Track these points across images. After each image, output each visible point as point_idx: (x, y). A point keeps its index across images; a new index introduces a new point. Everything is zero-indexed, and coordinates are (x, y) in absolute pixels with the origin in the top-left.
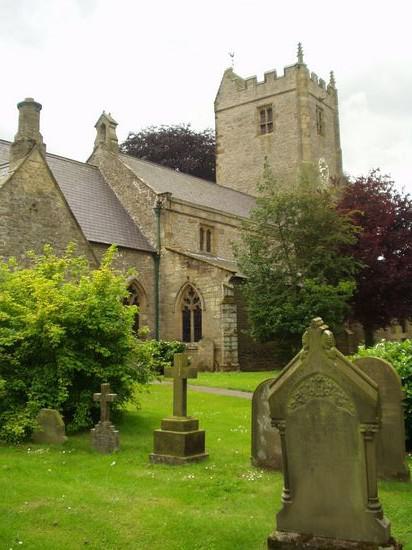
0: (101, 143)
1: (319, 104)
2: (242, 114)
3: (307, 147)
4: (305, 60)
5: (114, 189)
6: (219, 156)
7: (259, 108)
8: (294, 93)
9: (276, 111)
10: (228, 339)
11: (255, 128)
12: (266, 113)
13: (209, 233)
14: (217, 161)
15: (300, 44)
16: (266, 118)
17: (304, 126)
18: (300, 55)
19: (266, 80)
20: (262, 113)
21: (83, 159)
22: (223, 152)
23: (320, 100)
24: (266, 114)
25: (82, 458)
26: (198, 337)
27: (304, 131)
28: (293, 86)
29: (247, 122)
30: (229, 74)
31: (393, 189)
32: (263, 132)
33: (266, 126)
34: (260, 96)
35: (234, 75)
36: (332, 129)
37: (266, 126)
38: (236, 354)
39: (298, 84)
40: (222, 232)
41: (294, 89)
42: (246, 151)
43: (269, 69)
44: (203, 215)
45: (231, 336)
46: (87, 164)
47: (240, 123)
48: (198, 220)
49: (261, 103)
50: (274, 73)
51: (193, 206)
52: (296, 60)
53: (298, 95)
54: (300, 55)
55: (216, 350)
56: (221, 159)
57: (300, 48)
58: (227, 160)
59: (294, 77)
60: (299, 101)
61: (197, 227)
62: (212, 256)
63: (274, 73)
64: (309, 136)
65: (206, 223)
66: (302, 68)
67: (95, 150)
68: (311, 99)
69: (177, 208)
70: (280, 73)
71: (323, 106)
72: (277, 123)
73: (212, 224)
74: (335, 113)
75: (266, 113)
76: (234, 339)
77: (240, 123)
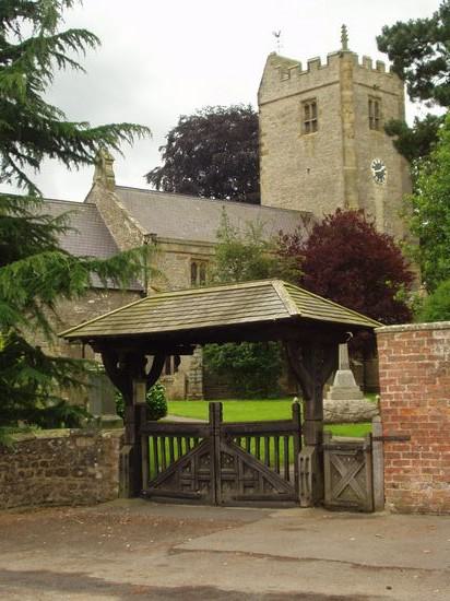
0: (99, 180)
1: (374, 93)
2: (286, 109)
3: (351, 150)
4: (351, 46)
5: (109, 227)
6: (263, 158)
7: (303, 102)
8: (338, 85)
9: (320, 107)
10: (193, 372)
11: (299, 126)
12: (310, 106)
14: (262, 164)
15: (344, 27)
16: (311, 114)
17: (347, 126)
18: (344, 39)
19: (309, 70)
20: (307, 108)
21: (81, 199)
23: (375, 88)
24: (311, 108)
25: (148, 503)
26: (176, 370)
27: (347, 132)
28: (337, 78)
29: (291, 119)
30: (273, 60)
32: (308, 131)
33: (311, 125)
34: (313, 86)
35: (280, 59)
37: (311, 125)
38: (200, 385)
39: (341, 76)
41: (337, 82)
42: (290, 152)
43: (312, 56)
44: (195, 250)
45: (195, 370)
46: (85, 203)
47: (283, 119)
48: (189, 256)
49: (305, 97)
50: (318, 61)
51: (181, 243)
52: (339, 47)
53: (342, 89)
54: (344, 39)
55: (187, 382)
56: (265, 163)
57: (344, 32)
58: (271, 163)
59: (337, 67)
60: (342, 97)
61: (187, 263)
63: (318, 61)
64: (353, 137)
65: (199, 257)
66: (346, 57)
67: (94, 185)
68: (360, 90)
69: (164, 247)
70: (324, 62)
71: (381, 94)
72: (321, 121)
75: (310, 106)
76: (199, 372)
77: (283, 119)
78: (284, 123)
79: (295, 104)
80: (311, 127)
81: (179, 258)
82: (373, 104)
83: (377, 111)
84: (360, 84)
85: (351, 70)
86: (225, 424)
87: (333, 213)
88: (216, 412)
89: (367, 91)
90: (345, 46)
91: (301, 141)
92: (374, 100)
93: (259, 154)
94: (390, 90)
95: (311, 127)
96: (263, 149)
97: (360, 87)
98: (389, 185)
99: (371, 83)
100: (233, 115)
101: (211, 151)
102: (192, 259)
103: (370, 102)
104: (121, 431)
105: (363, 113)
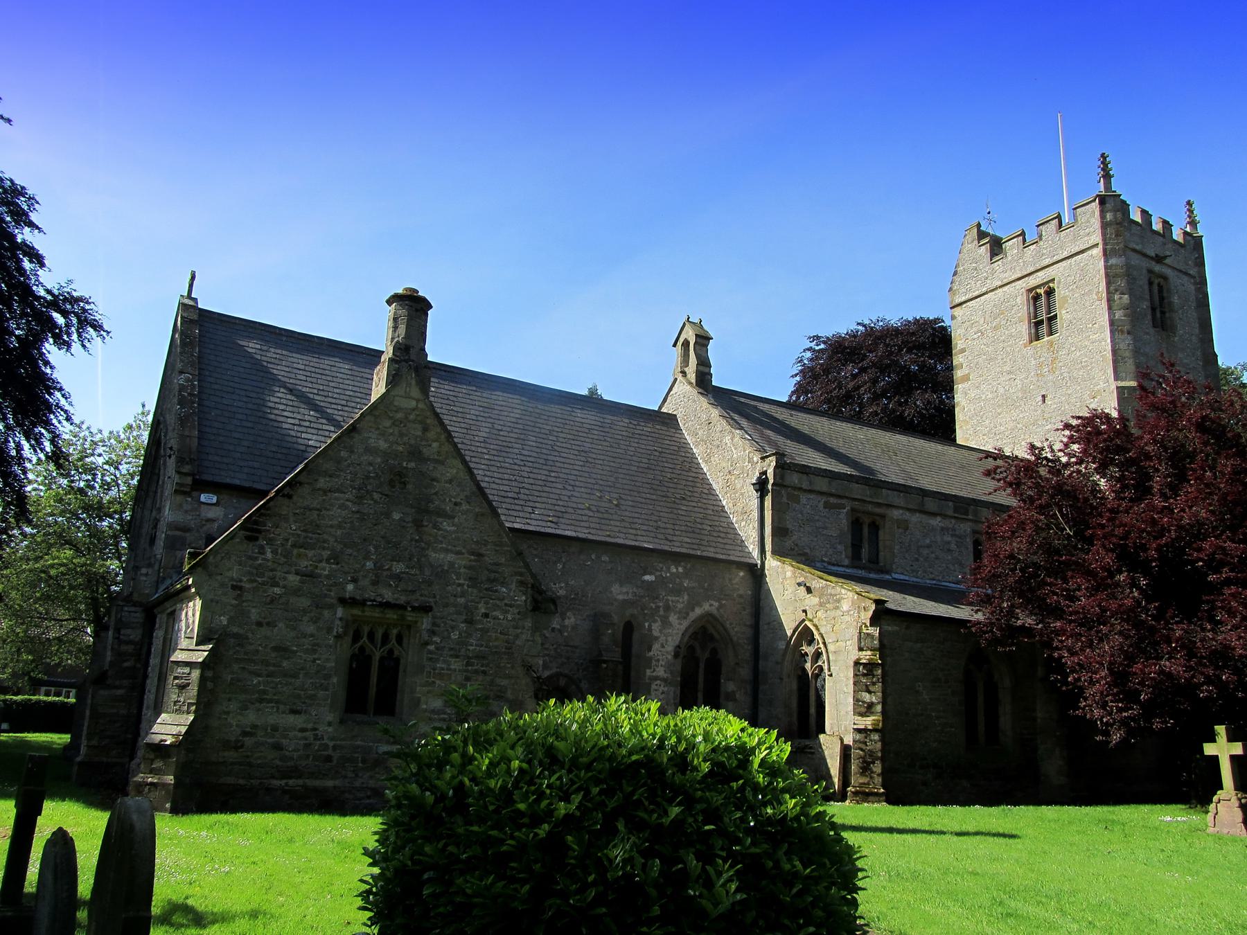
1: (1157, 268)
4: (1116, 187)
7: (1030, 290)
11: (1024, 329)
13: (875, 528)
16: (1044, 310)
18: (1107, 176)
22: (966, 378)
23: (1159, 259)
31: (94, 430)
36: (1193, 315)
40: (904, 525)
42: (1009, 373)
49: (1033, 281)
61: (842, 521)
62: (882, 572)
71: (1168, 272)
73: (878, 510)
74: (1201, 283)
78: (996, 328)
79: (1017, 297)
81: (827, 505)
82: (1156, 288)
83: (1162, 299)
86: (101, 805)
87: (859, 864)
88: (1047, 626)
89: (1146, 264)
90: (1108, 186)
92: (1156, 281)
94: (1181, 267)
95: (1045, 327)
96: (958, 374)
102: (853, 510)
103: (1151, 283)
104: (178, 656)
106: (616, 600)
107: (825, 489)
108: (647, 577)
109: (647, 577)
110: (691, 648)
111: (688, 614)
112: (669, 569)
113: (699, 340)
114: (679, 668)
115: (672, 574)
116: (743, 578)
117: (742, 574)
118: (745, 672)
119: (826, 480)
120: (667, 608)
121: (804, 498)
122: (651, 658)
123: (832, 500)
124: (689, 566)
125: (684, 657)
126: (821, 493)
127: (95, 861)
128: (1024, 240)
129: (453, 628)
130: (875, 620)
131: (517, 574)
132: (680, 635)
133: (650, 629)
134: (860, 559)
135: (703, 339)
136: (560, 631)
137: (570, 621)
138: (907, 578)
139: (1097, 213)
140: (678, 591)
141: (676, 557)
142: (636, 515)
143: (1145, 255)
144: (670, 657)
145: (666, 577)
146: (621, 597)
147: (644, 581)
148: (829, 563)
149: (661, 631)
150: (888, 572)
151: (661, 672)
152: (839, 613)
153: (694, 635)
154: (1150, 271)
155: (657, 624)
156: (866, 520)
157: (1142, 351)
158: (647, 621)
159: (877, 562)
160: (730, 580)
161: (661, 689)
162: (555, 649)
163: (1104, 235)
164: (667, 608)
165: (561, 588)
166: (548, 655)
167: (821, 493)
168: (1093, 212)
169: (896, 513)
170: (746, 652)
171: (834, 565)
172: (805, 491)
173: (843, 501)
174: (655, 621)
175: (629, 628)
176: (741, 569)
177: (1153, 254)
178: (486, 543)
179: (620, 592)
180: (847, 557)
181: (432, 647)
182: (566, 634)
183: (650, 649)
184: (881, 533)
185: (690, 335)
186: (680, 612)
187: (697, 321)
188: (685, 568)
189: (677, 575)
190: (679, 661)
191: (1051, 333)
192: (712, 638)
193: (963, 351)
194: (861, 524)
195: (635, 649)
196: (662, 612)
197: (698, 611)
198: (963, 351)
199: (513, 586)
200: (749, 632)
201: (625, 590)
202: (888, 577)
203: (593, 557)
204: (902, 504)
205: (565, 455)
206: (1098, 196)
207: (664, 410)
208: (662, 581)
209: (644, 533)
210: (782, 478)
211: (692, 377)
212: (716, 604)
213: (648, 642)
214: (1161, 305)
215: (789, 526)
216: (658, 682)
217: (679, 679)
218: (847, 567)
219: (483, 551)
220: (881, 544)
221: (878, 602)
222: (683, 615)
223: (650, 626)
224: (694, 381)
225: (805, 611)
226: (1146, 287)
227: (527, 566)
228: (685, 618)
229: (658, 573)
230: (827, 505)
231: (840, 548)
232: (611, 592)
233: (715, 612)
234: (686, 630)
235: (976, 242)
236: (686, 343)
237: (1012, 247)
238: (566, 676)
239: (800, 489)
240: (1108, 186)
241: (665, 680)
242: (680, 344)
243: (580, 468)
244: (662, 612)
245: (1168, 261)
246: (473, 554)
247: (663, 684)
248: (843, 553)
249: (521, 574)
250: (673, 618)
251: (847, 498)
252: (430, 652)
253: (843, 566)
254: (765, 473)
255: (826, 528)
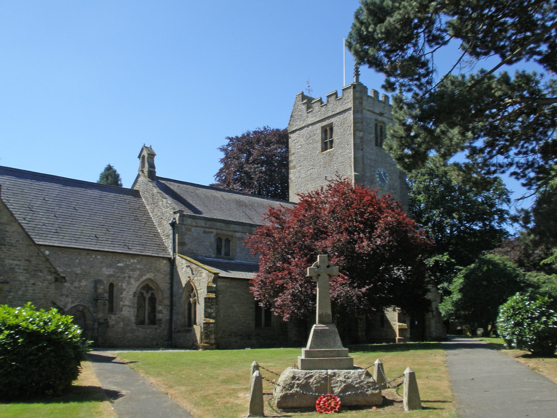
1: (380, 118)
4: (361, 80)
6: (291, 171)
11: (319, 145)
12: (327, 131)
13: (228, 241)
22: (294, 167)
33: (327, 144)
37: (327, 144)
48: (215, 231)
49: (324, 123)
62: (231, 260)
64: (362, 150)
66: (358, 89)
80: (329, 146)
81: (204, 232)
82: (379, 128)
84: (368, 110)
85: (361, 98)
89: (374, 117)
90: (357, 79)
91: (321, 156)
92: (379, 125)
93: (287, 169)
96: (291, 165)
97: (368, 113)
98: (390, 189)
99: (377, 111)
100: (288, 198)
101: (309, 292)
105: (370, 133)
106: (105, 274)
107: (203, 225)
108: (120, 265)
109: (120, 265)
110: (142, 294)
111: (139, 279)
112: (130, 261)
113: (150, 156)
114: (136, 301)
115: (132, 263)
116: (165, 263)
117: (165, 262)
118: (167, 302)
119: (204, 221)
120: (130, 277)
121: (193, 229)
122: (122, 298)
123: (207, 230)
124: (139, 259)
125: (138, 297)
126: (202, 227)
127: (300, 365)
128: (337, 97)
129: (19, 289)
130: (214, 281)
131: (47, 267)
132: (136, 287)
133: (121, 286)
134: (220, 254)
135: (152, 155)
136: (78, 287)
137: (84, 283)
138: (242, 262)
139: (352, 93)
140: (134, 270)
141: (134, 256)
142: (115, 238)
143: (374, 113)
144: (131, 297)
145: (129, 264)
146: (107, 273)
147: (118, 266)
148: (205, 256)
149: (127, 287)
150: (233, 259)
151: (127, 303)
152: (201, 278)
153: (143, 288)
154: (376, 120)
155: (125, 284)
156: (224, 238)
157: (369, 157)
158: (120, 282)
159: (229, 255)
160: (160, 264)
161: (128, 309)
162: (77, 295)
163: (354, 103)
164: (130, 277)
165: (78, 270)
166: (73, 298)
167: (202, 227)
168: (350, 93)
169: (238, 235)
170: (167, 294)
171: (207, 257)
172: (194, 226)
173: (212, 230)
174: (124, 283)
175: (112, 286)
176: (165, 260)
177: (378, 112)
178: (32, 256)
179: (107, 271)
180: (213, 254)
181: (10, 297)
182: (81, 289)
183: (121, 294)
184: (231, 244)
185: (145, 153)
186: (136, 278)
187: (149, 146)
188: (138, 260)
189: (134, 263)
190: (136, 298)
191: (331, 147)
192: (151, 289)
193: (294, 154)
194: (221, 240)
195: (115, 294)
196: (127, 279)
197: (144, 278)
198: (294, 154)
199: (46, 273)
200: (168, 286)
201: (109, 270)
202: (233, 261)
203: (93, 256)
204: (241, 230)
205: (81, 211)
206: (352, 84)
207: (135, 188)
208: (127, 266)
209: (118, 246)
210: (183, 221)
211: (146, 173)
212: (153, 275)
213: (121, 291)
214: (381, 136)
215: (186, 242)
216: (126, 307)
217: (136, 306)
218: (214, 258)
219: (31, 259)
220: (231, 248)
221: (215, 274)
222: (137, 280)
223: (121, 284)
224: (147, 175)
225: (189, 277)
226: (374, 128)
227: (51, 264)
228: (138, 281)
229: (125, 263)
230: (204, 232)
231: (210, 250)
232: (102, 271)
233: (152, 278)
234: (139, 286)
235: (301, 101)
236: (144, 157)
237: (316, 107)
238: (83, 306)
239: (191, 225)
240: (357, 79)
241: (129, 306)
242: (141, 157)
243: (88, 217)
244: (127, 279)
245: (385, 115)
246: (26, 260)
247: (128, 308)
248: (212, 253)
249: (50, 268)
250: (132, 281)
251: (214, 229)
252: (10, 299)
253: (212, 258)
254: (175, 219)
255: (204, 242)
